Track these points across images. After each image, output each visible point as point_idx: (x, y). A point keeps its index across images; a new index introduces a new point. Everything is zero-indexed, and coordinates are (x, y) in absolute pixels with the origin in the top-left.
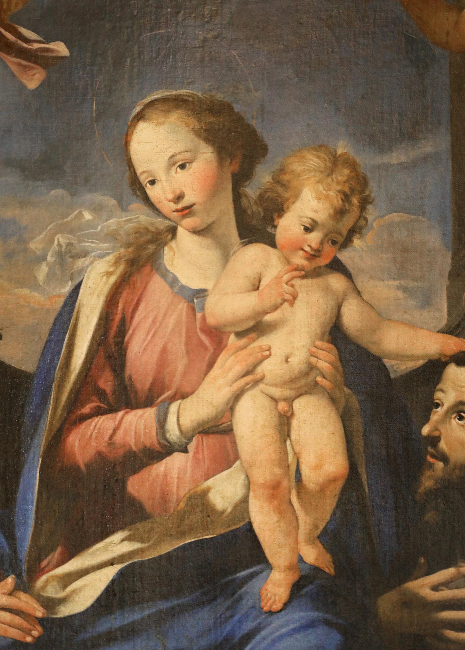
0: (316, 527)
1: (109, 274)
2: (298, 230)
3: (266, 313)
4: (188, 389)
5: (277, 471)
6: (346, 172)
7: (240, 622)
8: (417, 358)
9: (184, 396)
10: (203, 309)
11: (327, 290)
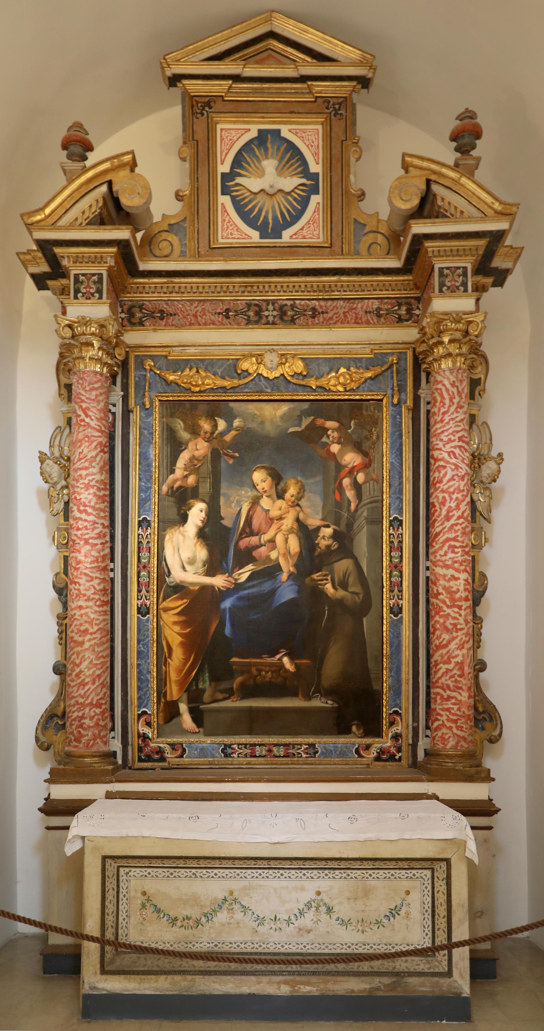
2: (289, 497)
9: (264, 533)
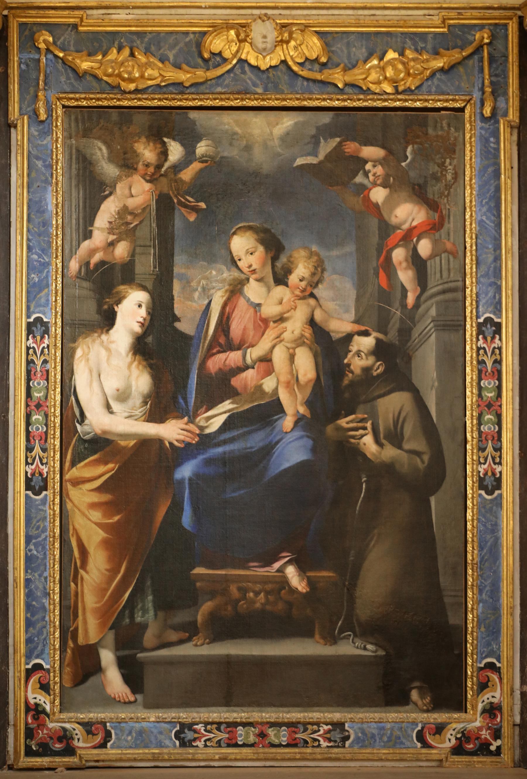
0: (304, 399)
1: (223, 296)
3: (285, 313)
4: (254, 343)
5: (289, 377)
6: (316, 258)
7: (275, 436)
8: (343, 332)
9: (253, 346)
10: (260, 311)
11: (308, 305)
